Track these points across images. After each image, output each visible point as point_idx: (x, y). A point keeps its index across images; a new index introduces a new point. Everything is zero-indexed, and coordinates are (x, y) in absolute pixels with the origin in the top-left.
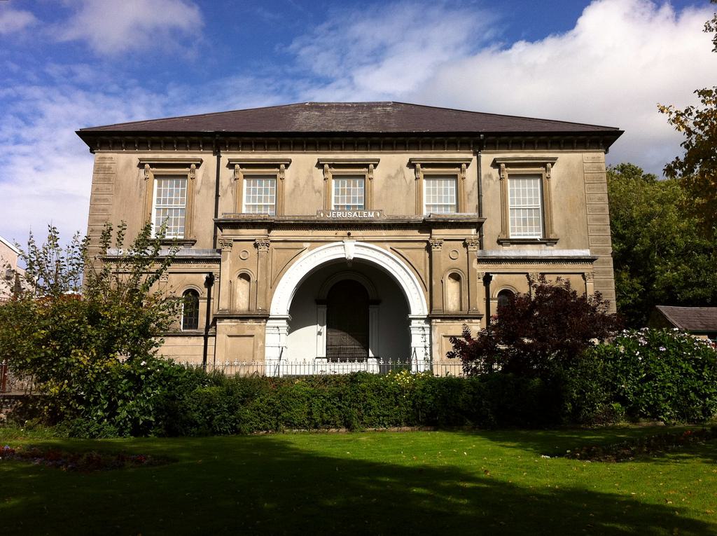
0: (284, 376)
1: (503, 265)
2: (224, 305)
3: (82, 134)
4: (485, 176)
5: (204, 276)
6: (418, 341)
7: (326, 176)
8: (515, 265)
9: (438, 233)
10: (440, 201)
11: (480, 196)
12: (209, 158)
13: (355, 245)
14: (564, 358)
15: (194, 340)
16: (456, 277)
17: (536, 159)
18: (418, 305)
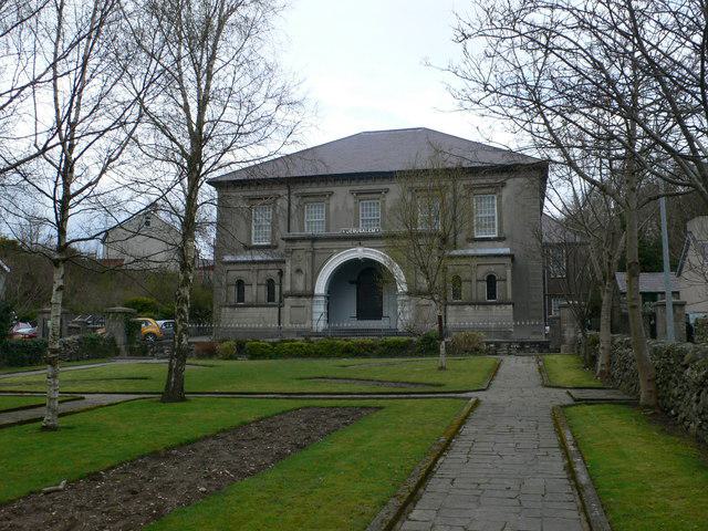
15: (271, 309)
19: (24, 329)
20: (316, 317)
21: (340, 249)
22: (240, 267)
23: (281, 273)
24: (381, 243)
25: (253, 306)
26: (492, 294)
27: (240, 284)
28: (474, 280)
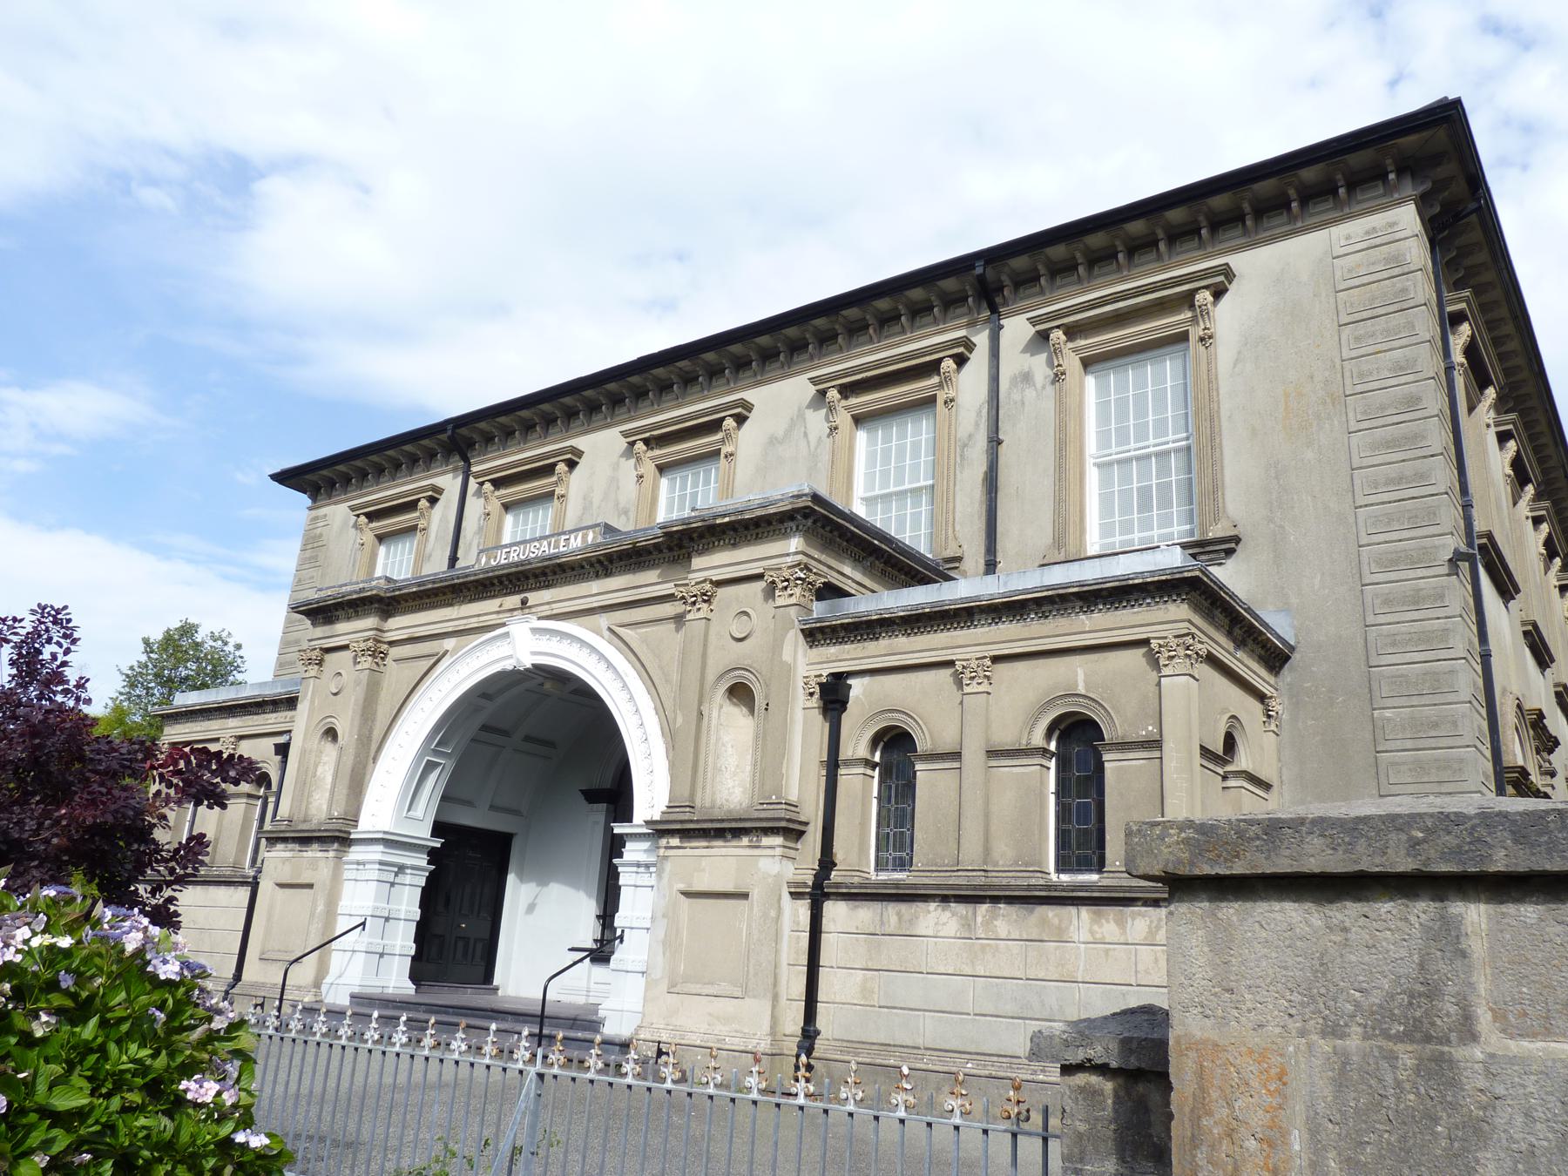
1: (884, 644)
3: (287, 478)
4: (1013, 381)
7: (642, 471)
8: (920, 638)
10: (900, 481)
11: (995, 442)
12: (449, 482)
13: (534, 631)
14: (213, 772)
16: (740, 693)
17: (1164, 285)
18: (651, 796)
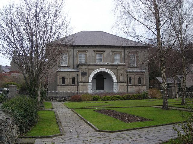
0: (11, 64)
2: (80, 80)
5: (76, 75)
6: (115, 86)
9: (119, 67)
15: (75, 86)
18: (115, 80)
19: (27, 97)
20: (89, 89)
21: (97, 68)
22: (63, 73)
23: (77, 75)
24: (109, 67)
25: (67, 86)
26: (140, 83)
27: (63, 79)
28: (69, 79)
